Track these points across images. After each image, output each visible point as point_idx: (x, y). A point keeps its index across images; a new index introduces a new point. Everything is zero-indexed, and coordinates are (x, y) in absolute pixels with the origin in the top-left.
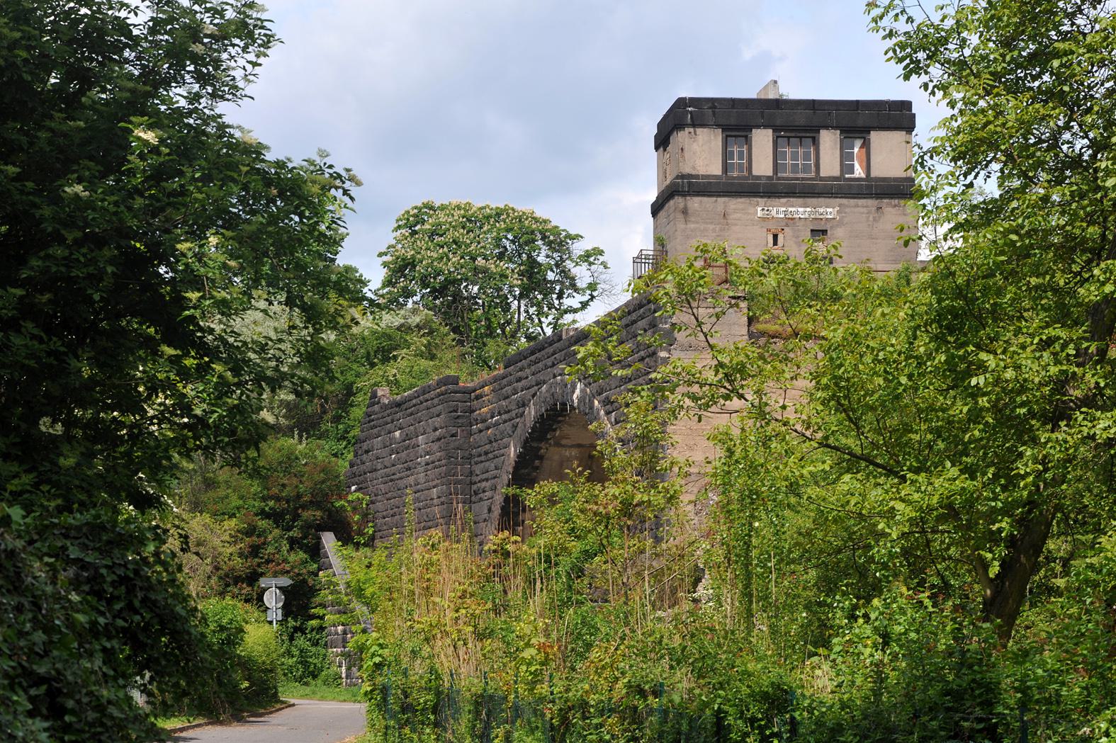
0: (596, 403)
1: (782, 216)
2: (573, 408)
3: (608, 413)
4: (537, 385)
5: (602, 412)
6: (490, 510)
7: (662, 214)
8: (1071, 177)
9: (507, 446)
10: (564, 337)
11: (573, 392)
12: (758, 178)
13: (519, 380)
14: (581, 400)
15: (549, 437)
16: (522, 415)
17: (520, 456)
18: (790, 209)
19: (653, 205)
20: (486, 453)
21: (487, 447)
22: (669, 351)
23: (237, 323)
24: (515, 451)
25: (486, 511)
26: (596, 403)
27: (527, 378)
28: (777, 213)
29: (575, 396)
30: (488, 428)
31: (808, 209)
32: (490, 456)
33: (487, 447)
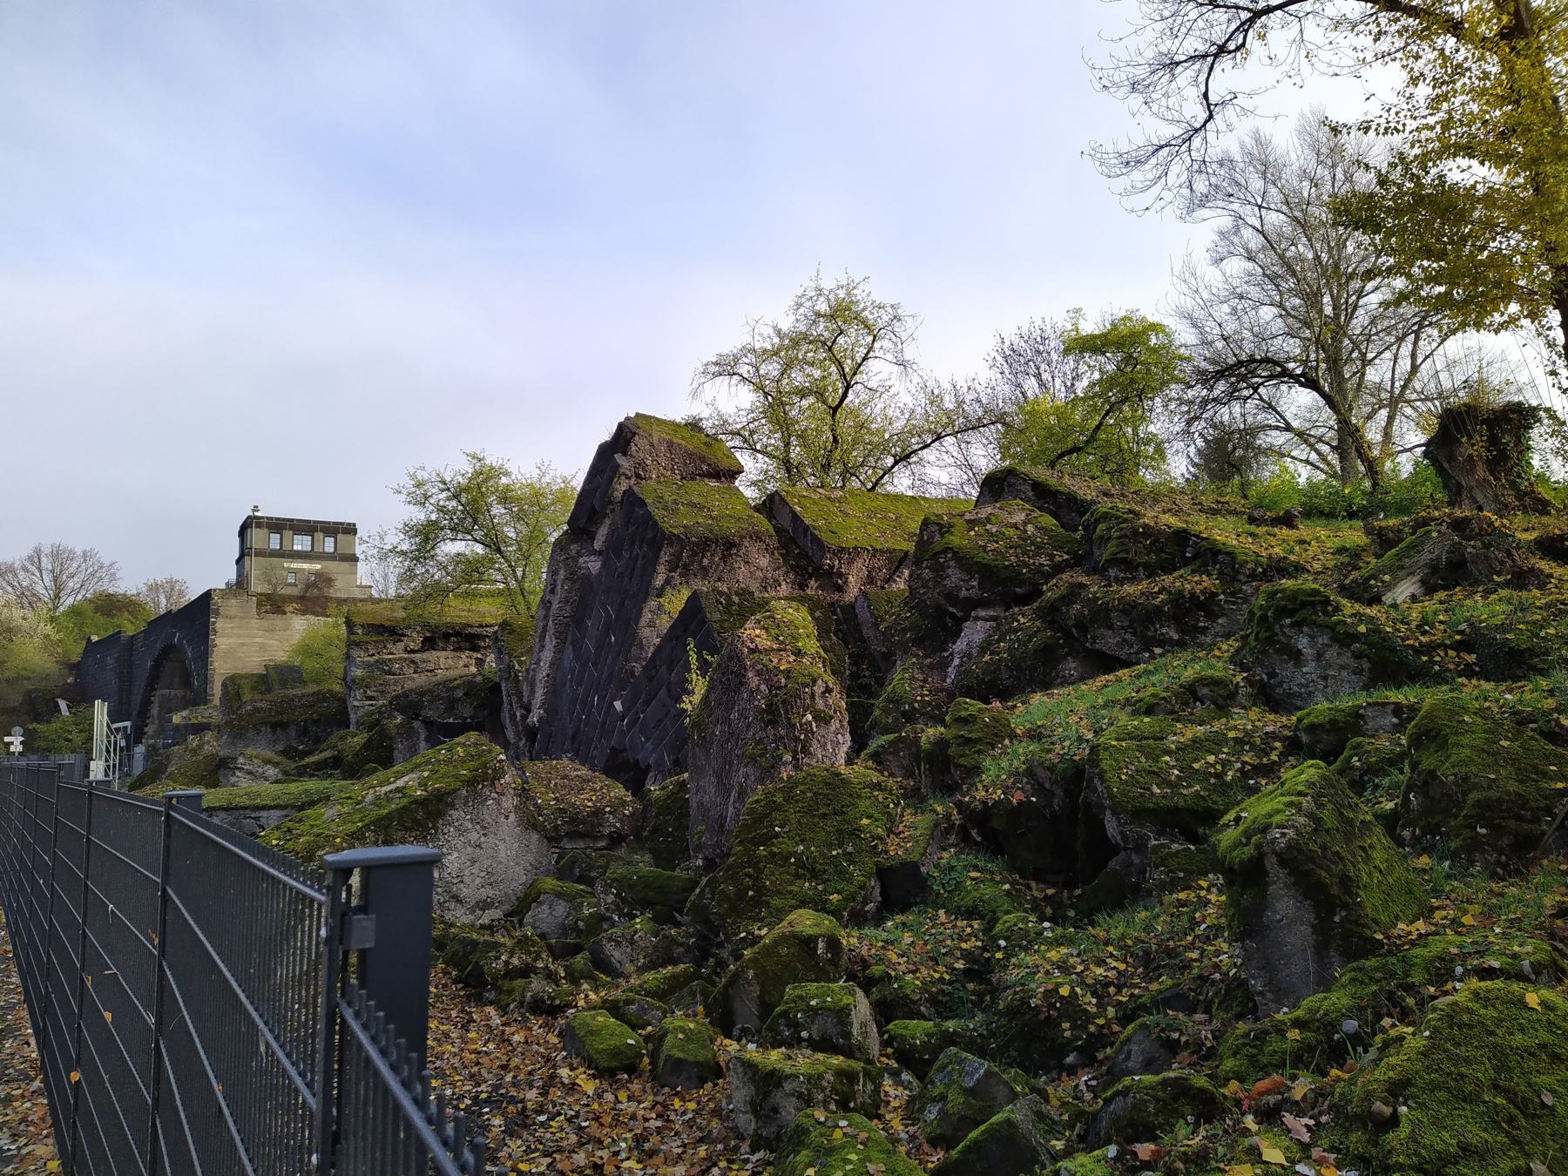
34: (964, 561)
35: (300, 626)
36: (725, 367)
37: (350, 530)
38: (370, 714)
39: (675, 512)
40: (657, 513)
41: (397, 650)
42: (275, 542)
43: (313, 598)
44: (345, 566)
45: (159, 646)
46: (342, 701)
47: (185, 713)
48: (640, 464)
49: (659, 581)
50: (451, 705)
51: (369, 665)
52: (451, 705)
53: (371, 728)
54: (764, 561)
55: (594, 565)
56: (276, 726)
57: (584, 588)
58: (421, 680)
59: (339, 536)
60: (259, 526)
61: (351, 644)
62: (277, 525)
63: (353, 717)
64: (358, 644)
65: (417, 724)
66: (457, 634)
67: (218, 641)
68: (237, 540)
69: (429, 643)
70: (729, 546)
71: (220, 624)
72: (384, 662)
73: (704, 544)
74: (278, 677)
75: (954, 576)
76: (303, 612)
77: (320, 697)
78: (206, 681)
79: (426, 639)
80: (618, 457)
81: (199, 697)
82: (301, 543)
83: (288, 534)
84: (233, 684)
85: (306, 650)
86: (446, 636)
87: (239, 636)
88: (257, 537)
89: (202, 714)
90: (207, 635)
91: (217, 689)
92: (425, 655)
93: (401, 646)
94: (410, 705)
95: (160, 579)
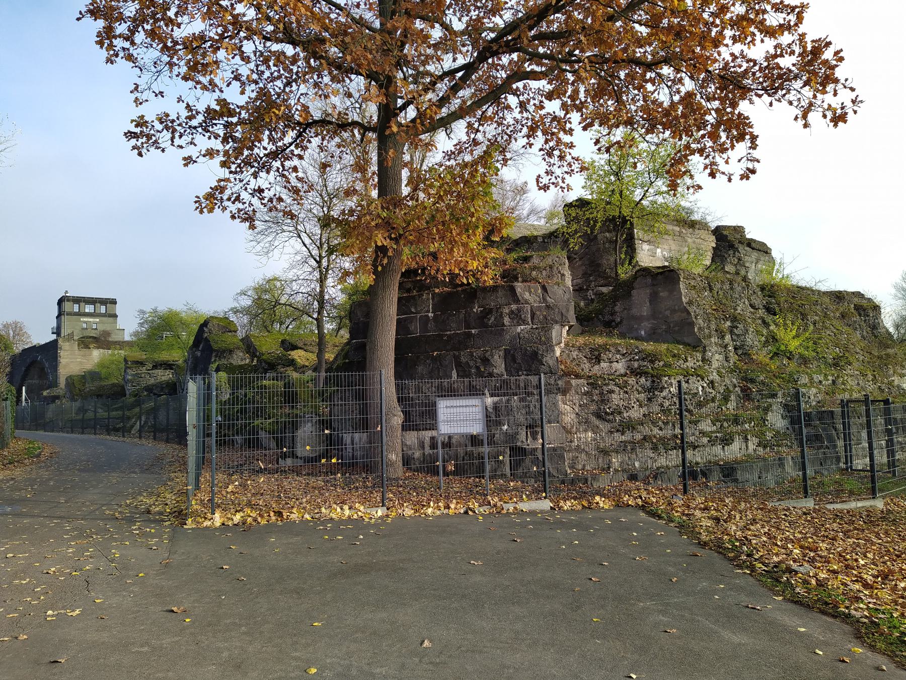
34: (265, 361)
35: (96, 355)
36: (243, 293)
37: (114, 302)
38: (134, 391)
39: (217, 343)
40: (212, 344)
41: (144, 369)
42: (76, 308)
43: (101, 341)
44: (111, 319)
45: (28, 361)
46: (123, 388)
47: (48, 391)
48: (211, 330)
49: (213, 360)
50: (162, 389)
51: (133, 375)
52: (162, 389)
53: (135, 396)
54: (241, 354)
55: (199, 354)
56: (99, 396)
57: (195, 358)
58: (152, 381)
59: (108, 305)
60: (68, 300)
61: (126, 368)
62: (77, 300)
63: (127, 392)
64: (129, 368)
65: (151, 394)
66: (165, 364)
67: (61, 361)
68: (57, 307)
69: (155, 367)
70: (231, 352)
71: (62, 353)
72: (139, 374)
73: (224, 351)
74: (92, 375)
75: (263, 364)
76: (98, 348)
77: (114, 385)
78: (56, 377)
79: (153, 366)
80: (205, 329)
81: (54, 384)
82: (89, 309)
83: (82, 304)
84: (70, 381)
85: (101, 365)
86: (161, 365)
87: (71, 359)
88: (67, 306)
89: (55, 392)
90: (57, 358)
91: (62, 382)
92: (153, 371)
93: (144, 368)
94: (149, 389)
95: (10, 321)
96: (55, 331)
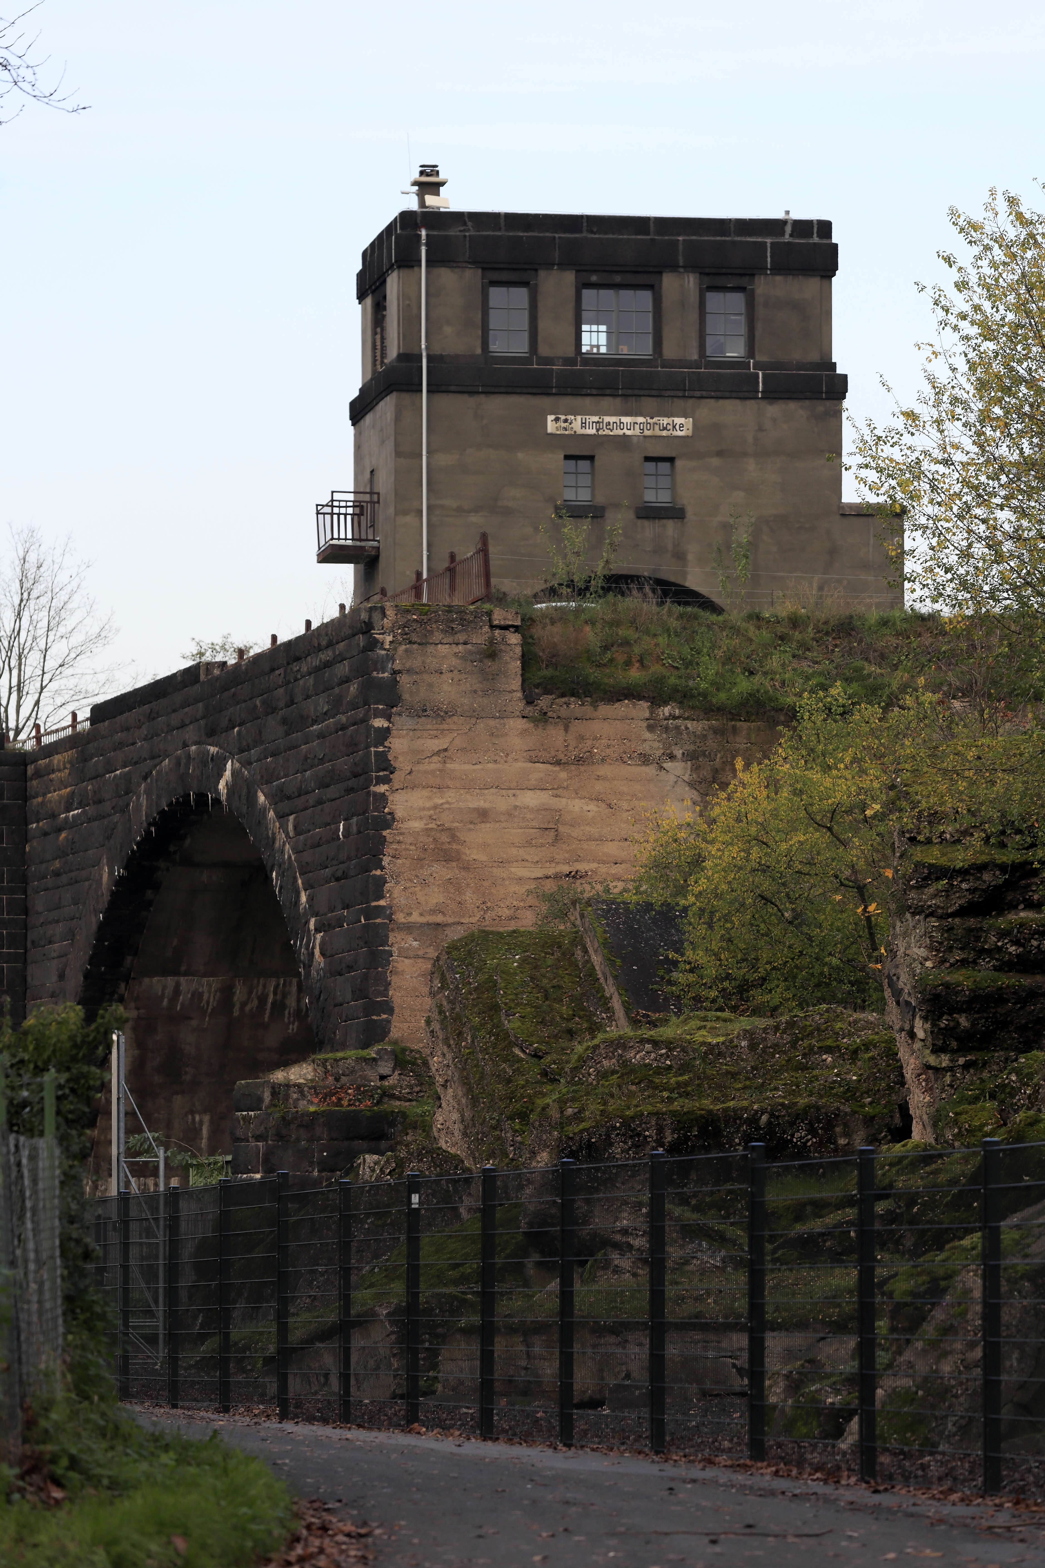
0: (262, 798)
1: (593, 431)
2: (217, 801)
3: (282, 816)
4: (153, 758)
5: (271, 814)
6: (62, 976)
7: (369, 419)
8: (65, 1339)
9: (97, 863)
10: (202, 677)
11: (220, 776)
12: (548, 361)
13: (121, 745)
14: (232, 789)
15: (172, 849)
16: (124, 809)
17: (120, 882)
18: (607, 419)
19: (353, 405)
20: (57, 874)
21: (57, 864)
22: (389, 718)
23: (462, 1154)
24: (111, 872)
25: (55, 978)
26: (262, 798)
27: (134, 744)
28: (583, 425)
29: (222, 785)
30: (59, 830)
31: (641, 419)
32: (64, 879)
33: (57, 864)
96: (345, 532)
